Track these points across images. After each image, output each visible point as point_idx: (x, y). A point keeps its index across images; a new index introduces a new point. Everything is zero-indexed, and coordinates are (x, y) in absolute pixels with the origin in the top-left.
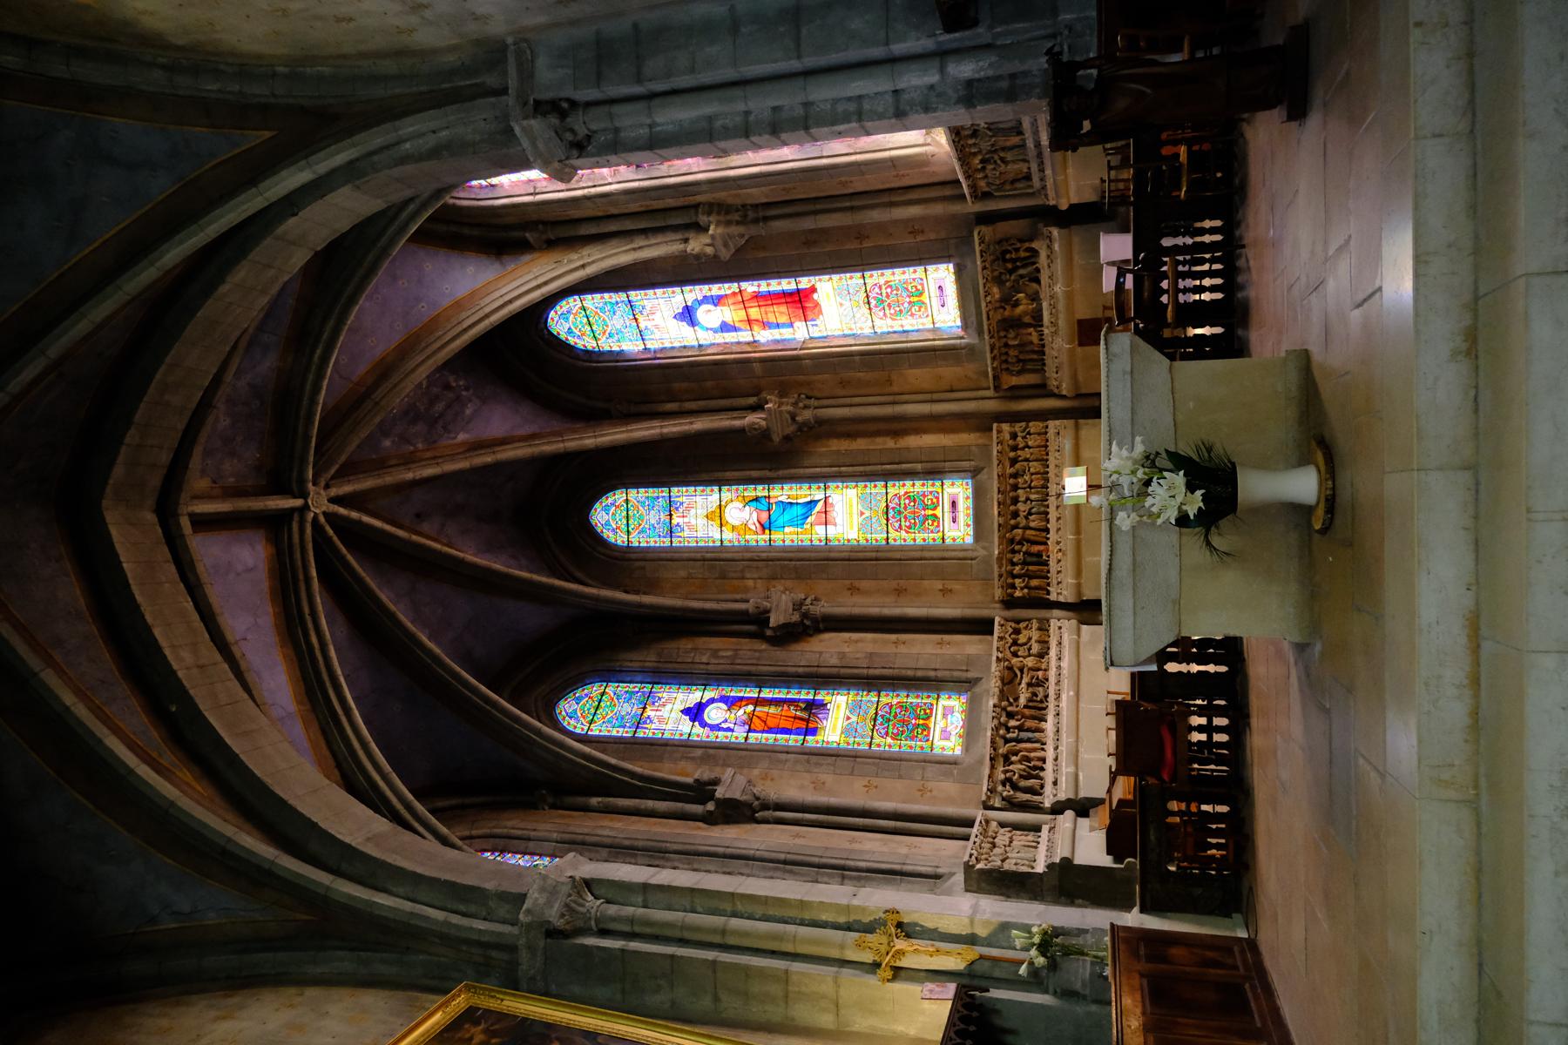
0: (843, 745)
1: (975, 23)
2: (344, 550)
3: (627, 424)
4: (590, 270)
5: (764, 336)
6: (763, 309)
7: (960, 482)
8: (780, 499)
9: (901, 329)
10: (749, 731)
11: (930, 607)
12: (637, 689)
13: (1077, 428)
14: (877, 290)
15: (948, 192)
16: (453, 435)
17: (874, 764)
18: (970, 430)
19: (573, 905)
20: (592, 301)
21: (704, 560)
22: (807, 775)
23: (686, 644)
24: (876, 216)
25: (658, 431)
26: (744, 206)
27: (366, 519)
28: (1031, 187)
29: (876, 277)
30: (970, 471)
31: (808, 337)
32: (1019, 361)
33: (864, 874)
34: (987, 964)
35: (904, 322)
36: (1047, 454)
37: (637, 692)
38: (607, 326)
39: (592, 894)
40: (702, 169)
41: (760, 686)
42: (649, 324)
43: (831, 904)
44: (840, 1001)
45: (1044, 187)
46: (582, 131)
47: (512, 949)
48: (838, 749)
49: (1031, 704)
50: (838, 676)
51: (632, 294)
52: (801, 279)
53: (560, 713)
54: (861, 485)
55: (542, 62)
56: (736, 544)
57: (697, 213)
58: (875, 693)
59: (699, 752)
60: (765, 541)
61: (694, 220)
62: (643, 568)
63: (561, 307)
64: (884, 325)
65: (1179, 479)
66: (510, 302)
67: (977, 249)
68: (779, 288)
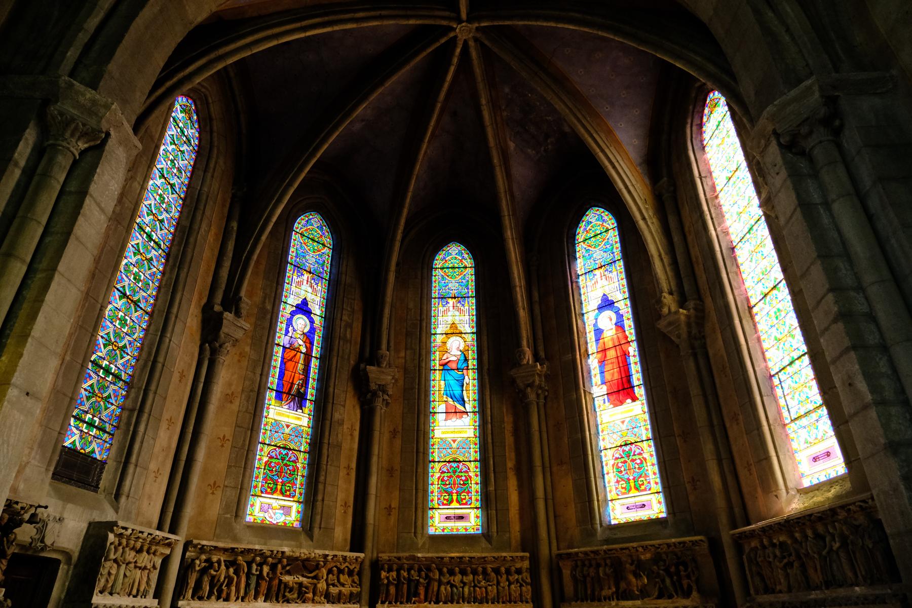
0: (264, 420)
2: (430, 50)
5: (593, 362)
6: (615, 360)
7: (480, 523)
8: (466, 377)
9: (605, 472)
10: (284, 348)
11: (376, 496)
12: (325, 269)
14: (638, 451)
17: (243, 445)
18: (523, 531)
19: (73, 126)
20: (614, 236)
21: (421, 321)
23: (357, 305)
24: (708, 448)
25: (518, 283)
26: (704, 337)
27: (452, 69)
28: (757, 593)
29: (649, 451)
30: (488, 532)
31: (594, 396)
33: (132, 428)
35: (611, 475)
36: (503, 603)
37: (323, 269)
38: (595, 247)
39: (86, 150)
40: (737, 298)
41: (322, 359)
43: (16, 366)
48: (261, 416)
49: (283, 586)
50: (324, 419)
51: (621, 263)
52: (643, 388)
53: (311, 215)
56: (433, 345)
58: (308, 449)
59: (269, 307)
60: (434, 366)
63: (607, 215)
64: (608, 459)
66: (614, 167)
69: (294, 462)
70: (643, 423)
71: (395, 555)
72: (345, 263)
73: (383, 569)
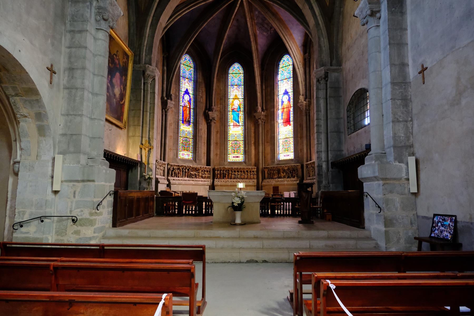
1: (332, 168)
3: (260, 75)
4: (297, 70)
5: (280, 112)
6: (286, 112)
8: (240, 114)
9: (280, 145)
10: (183, 106)
13: (254, 186)
14: (289, 140)
15: (309, 158)
16: (258, 29)
18: (255, 161)
19: (150, 77)
21: (225, 94)
22: (173, 122)
23: (204, 89)
24: (305, 142)
25: (258, 84)
26: (310, 110)
27: (237, 8)
28: (264, 178)
29: (292, 140)
32: (270, 173)
34: (144, 167)
41: (193, 109)
42: (285, 82)
44: (134, 137)
45: (307, 180)
46: (321, 82)
47: (139, 63)
51: (292, 79)
54: (243, 134)
55: (336, 74)
56: (229, 102)
57: (309, 98)
59: (177, 94)
61: (308, 97)
62: (223, 78)
64: (281, 142)
65: (240, 202)
66: (291, 49)
67: (296, 165)
68: (291, 116)
69: (189, 141)
70: (291, 133)
71: (219, 167)
72: (199, 74)
73: (216, 170)
